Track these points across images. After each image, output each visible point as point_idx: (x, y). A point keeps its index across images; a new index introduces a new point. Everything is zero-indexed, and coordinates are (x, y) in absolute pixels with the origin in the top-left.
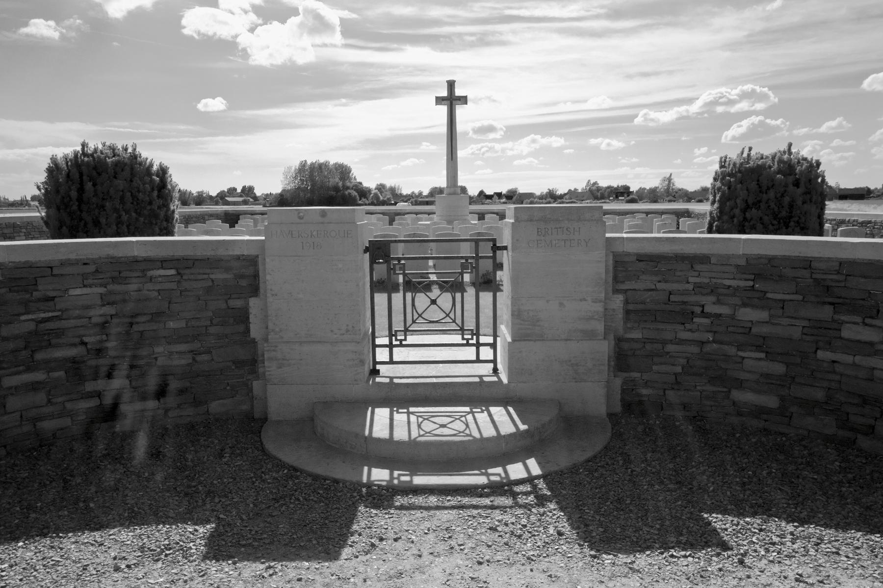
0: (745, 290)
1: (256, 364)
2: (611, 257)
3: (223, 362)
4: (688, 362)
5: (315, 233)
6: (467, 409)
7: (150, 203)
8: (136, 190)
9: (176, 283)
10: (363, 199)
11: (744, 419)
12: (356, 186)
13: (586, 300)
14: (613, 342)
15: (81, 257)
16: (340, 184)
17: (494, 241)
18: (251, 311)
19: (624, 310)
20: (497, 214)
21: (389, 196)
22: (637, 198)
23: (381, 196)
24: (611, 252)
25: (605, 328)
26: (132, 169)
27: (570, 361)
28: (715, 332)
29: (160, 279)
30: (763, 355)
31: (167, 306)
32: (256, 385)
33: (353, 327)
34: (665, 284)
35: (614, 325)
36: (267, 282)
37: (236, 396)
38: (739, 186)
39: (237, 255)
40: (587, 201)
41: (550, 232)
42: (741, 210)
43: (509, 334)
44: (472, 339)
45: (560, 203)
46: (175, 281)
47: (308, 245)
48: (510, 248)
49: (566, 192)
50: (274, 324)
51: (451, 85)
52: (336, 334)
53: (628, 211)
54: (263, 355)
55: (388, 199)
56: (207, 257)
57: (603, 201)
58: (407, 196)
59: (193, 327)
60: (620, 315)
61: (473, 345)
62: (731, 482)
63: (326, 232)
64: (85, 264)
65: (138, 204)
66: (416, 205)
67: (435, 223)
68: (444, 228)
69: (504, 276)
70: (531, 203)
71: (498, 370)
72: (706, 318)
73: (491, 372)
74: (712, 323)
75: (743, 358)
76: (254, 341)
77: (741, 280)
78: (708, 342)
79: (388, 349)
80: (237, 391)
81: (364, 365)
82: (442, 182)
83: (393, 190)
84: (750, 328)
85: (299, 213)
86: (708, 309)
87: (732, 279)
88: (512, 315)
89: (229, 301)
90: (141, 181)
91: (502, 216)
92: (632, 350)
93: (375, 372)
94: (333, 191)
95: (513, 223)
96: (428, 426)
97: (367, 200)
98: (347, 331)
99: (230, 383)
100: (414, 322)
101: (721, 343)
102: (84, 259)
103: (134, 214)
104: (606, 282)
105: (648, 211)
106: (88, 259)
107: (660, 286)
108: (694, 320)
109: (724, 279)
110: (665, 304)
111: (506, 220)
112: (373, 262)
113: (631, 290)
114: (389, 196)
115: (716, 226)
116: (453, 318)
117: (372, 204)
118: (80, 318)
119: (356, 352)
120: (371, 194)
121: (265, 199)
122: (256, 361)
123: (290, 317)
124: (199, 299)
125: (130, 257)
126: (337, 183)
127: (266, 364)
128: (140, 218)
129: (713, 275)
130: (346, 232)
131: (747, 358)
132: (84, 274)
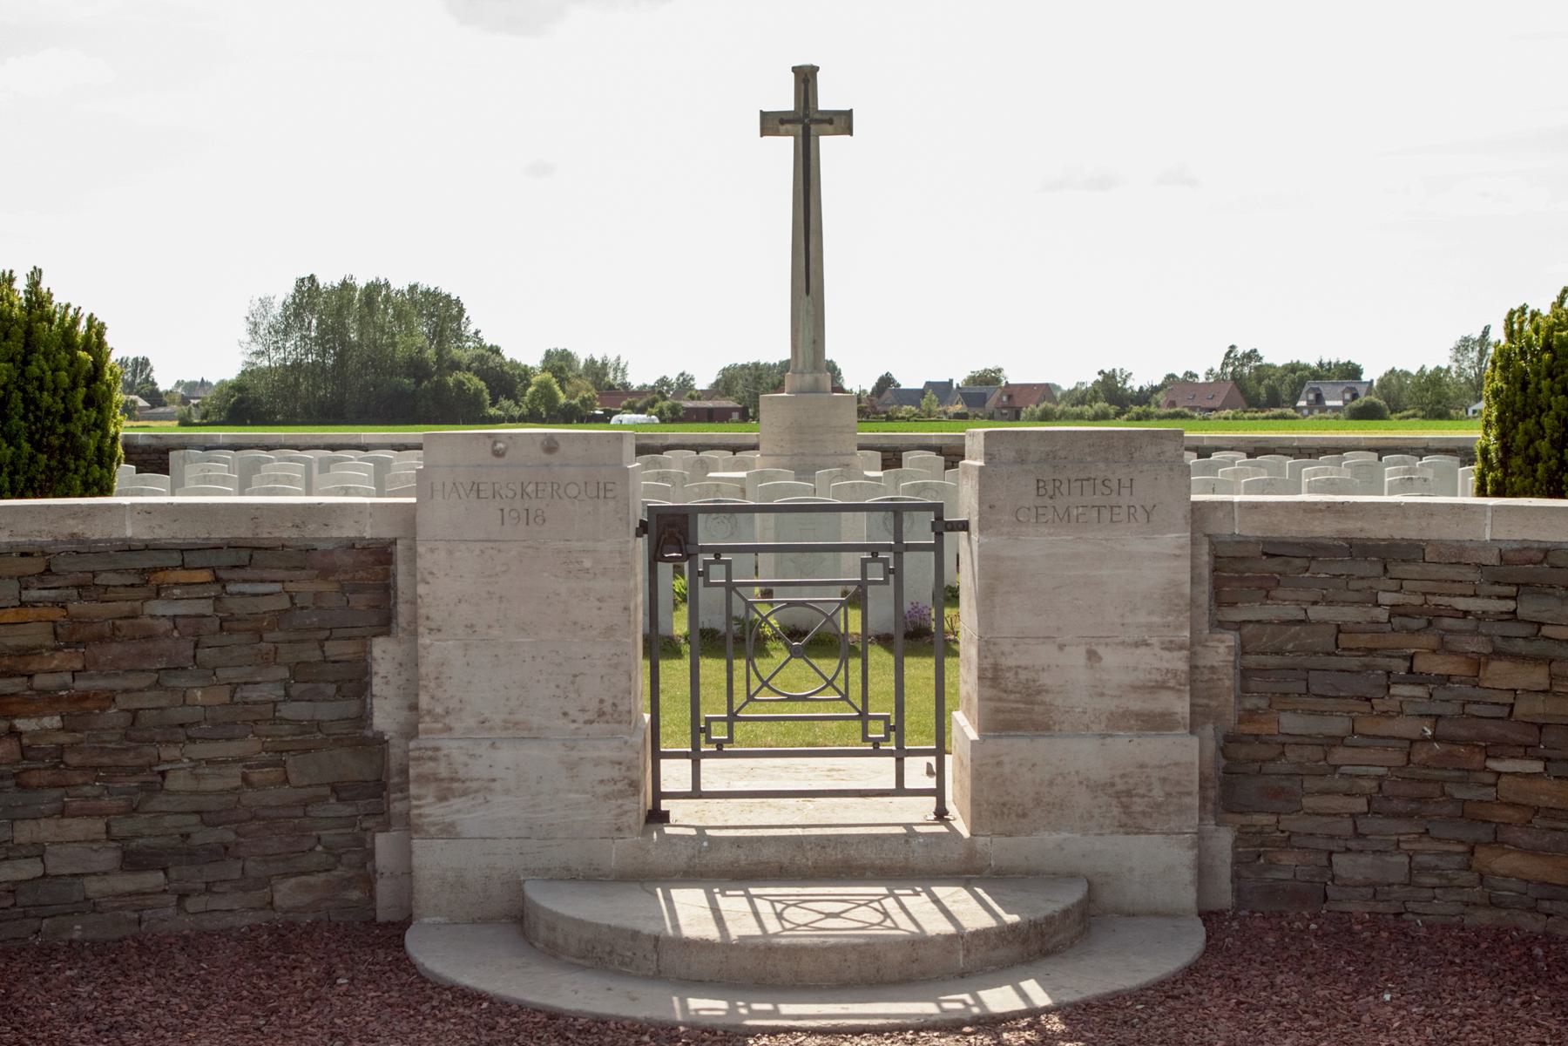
0: (1499, 620)
1: (385, 793)
2: (1205, 548)
3: (310, 786)
4: (1380, 787)
5: (531, 488)
6: (883, 890)
7: (67, 417)
8: (36, 384)
9: (211, 601)
10: (505, 403)
11: (1504, 913)
12: (481, 358)
13: (1147, 645)
14: (1211, 746)
15: (19, 539)
16: (430, 353)
17: (938, 509)
18: (375, 668)
19: (1235, 668)
20: (939, 450)
21: (587, 390)
22: (1383, 403)
23: (560, 394)
24: (1206, 535)
25: (1192, 713)
26: (29, 332)
27: (1113, 785)
28: (1438, 717)
29: (177, 592)
30: (1537, 767)
31: (191, 653)
32: (384, 845)
33: (614, 705)
34: (1327, 608)
35: (1213, 703)
36: (419, 600)
37: (336, 868)
38: (1545, 384)
39: (348, 539)
40: (1224, 413)
41: (1064, 489)
42: (1552, 442)
43: (972, 723)
44: (887, 739)
45: (1139, 418)
46: (209, 598)
47: (514, 514)
48: (974, 525)
49: (1158, 382)
50: (433, 698)
51: (806, 78)
52: (574, 721)
53: (1325, 444)
54: (404, 771)
55: (584, 401)
56: (279, 543)
57: (1277, 411)
58: (642, 392)
59: (247, 703)
60: (1228, 682)
61: (889, 753)
62: (1441, 1017)
63: (555, 487)
64: (23, 554)
65: (37, 419)
66: (673, 421)
67: (762, 476)
68: (791, 490)
69: (966, 621)
70: (1046, 417)
71: (947, 813)
72: (1420, 684)
73: (933, 817)
74: (1431, 695)
75: (1499, 774)
76: (380, 741)
77: (1490, 597)
78: (1425, 740)
79: (689, 761)
80: (340, 856)
81: (639, 795)
82: (774, 347)
83: (596, 371)
84: (1512, 706)
85: (495, 443)
86: (1420, 665)
87: (1472, 596)
88: (980, 678)
89: (327, 644)
90: (47, 361)
91: (952, 455)
92: (1254, 761)
93: (658, 817)
94: (407, 376)
95: (981, 468)
96: (795, 915)
97: (517, 404)
98: (601, 714)
99: (323, 840)
100: (751, 698)
101: (1453, 741)
102: (24, 544)
103: (26, 447)
104: (1193, 602)
105: (1383, 444)
106: (32, 544)
107: (1317, 613)
108: (1392, 691)
109: (1455, 596)
110: (1329, 654)
111: (966, 462)
112: (655, 557)
113: (1250, 622)
114: (587, 390)
115: (1494, 481)
116: (842, 688)
117: (532, 417)
118: (10, 677)
119: (620, 764)
120: (529, 385)
121: (185, 401)
122: (384, 787)
123: (469, 682)
124: (261, 639)
125: (116, 540)
126: (421, 350)
127: (413, 790)
128: (40, 456)
129: (1430, 586)
130: (602, 486)
131: (1506, 773)
132: (23, 577)
